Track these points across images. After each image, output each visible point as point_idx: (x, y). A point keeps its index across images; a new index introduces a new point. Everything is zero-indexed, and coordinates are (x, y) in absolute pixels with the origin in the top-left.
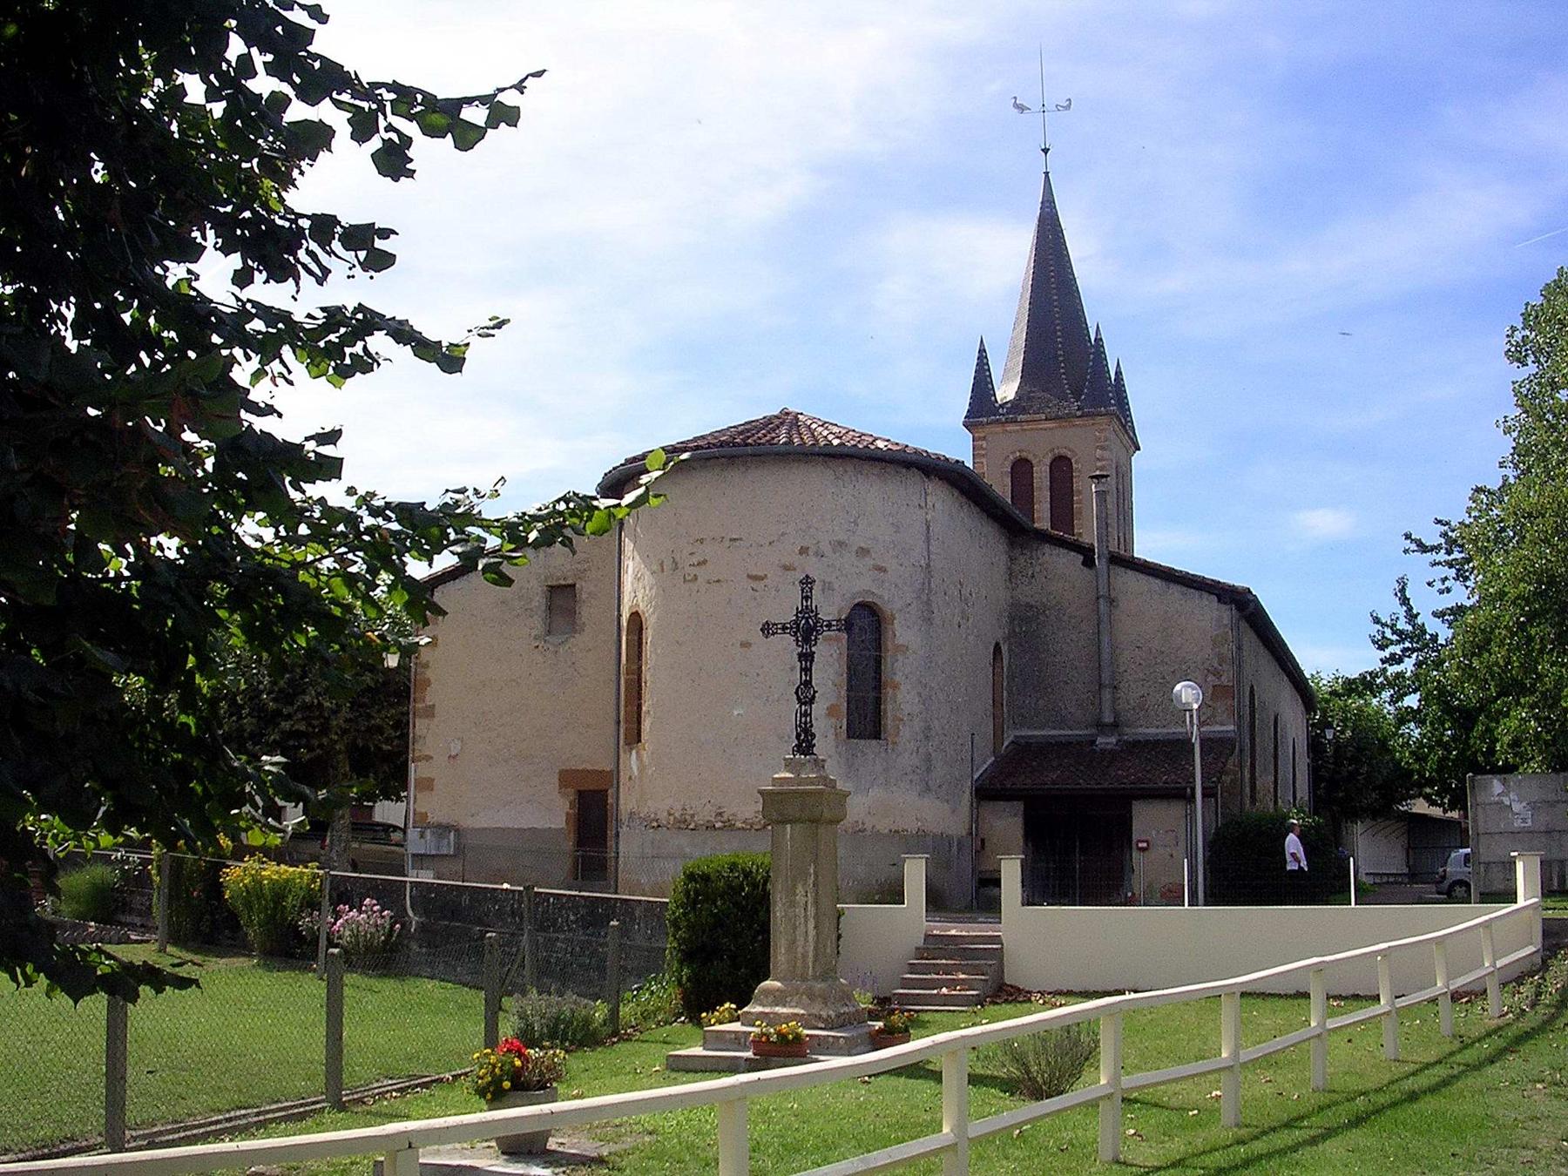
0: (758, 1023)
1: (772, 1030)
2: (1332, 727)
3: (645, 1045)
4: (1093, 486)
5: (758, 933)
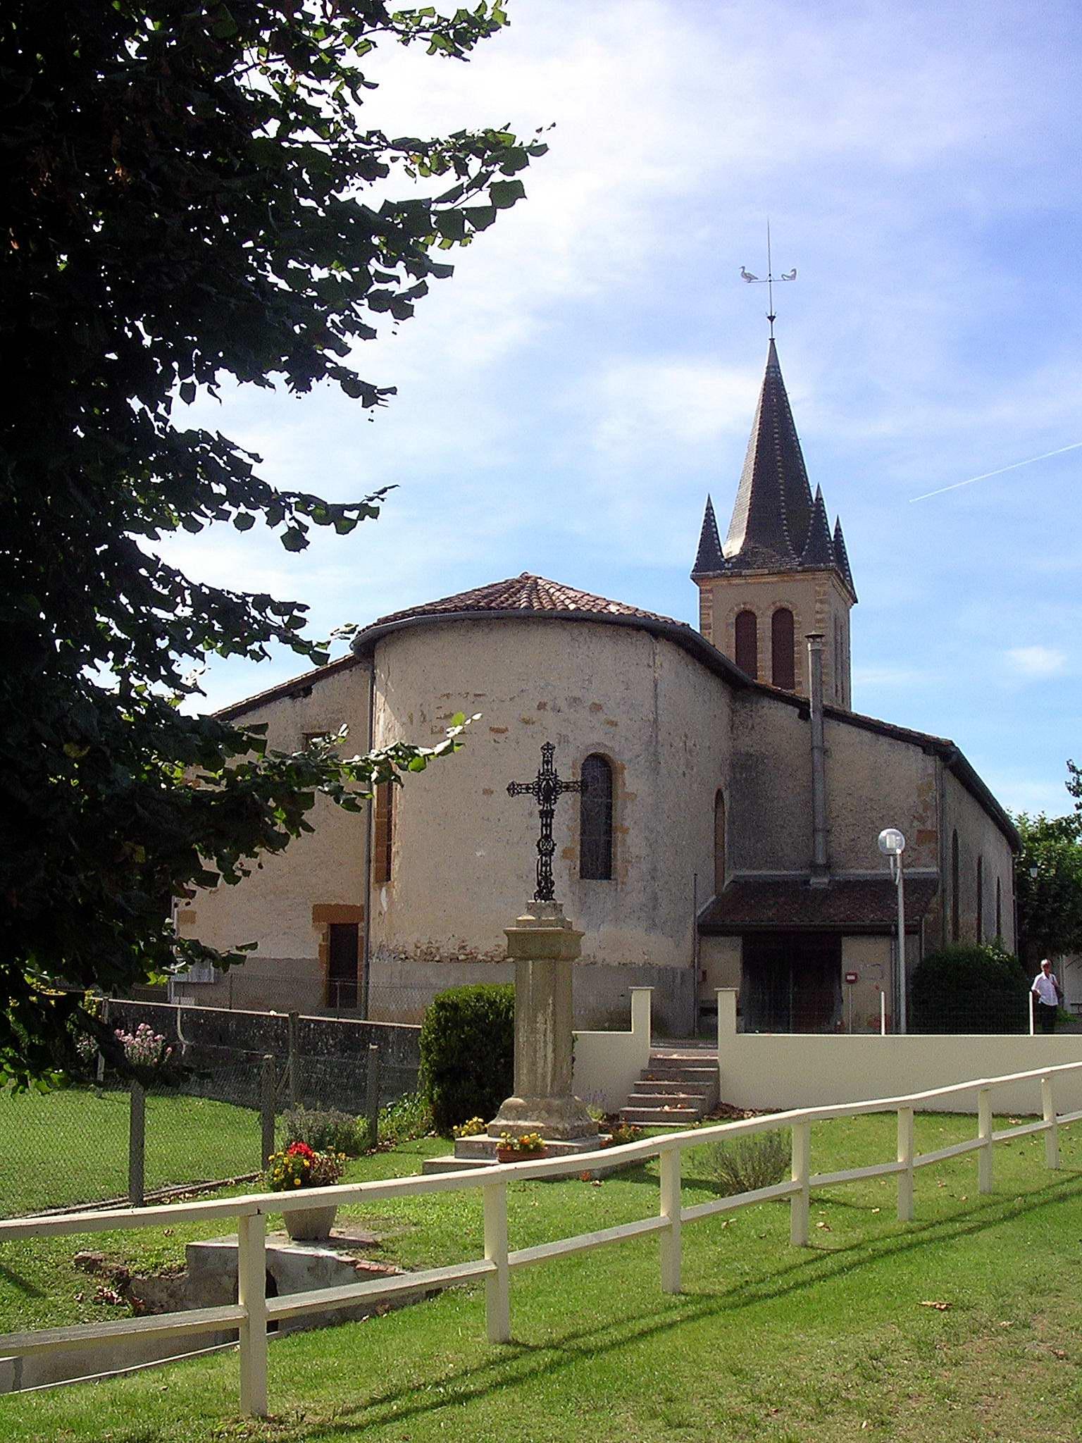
0: (503, 1134)
1: (516, 1141)
2: (1036, 866)
3: (402, 1155)
4: (809, 645)
5: (501, 1056)
